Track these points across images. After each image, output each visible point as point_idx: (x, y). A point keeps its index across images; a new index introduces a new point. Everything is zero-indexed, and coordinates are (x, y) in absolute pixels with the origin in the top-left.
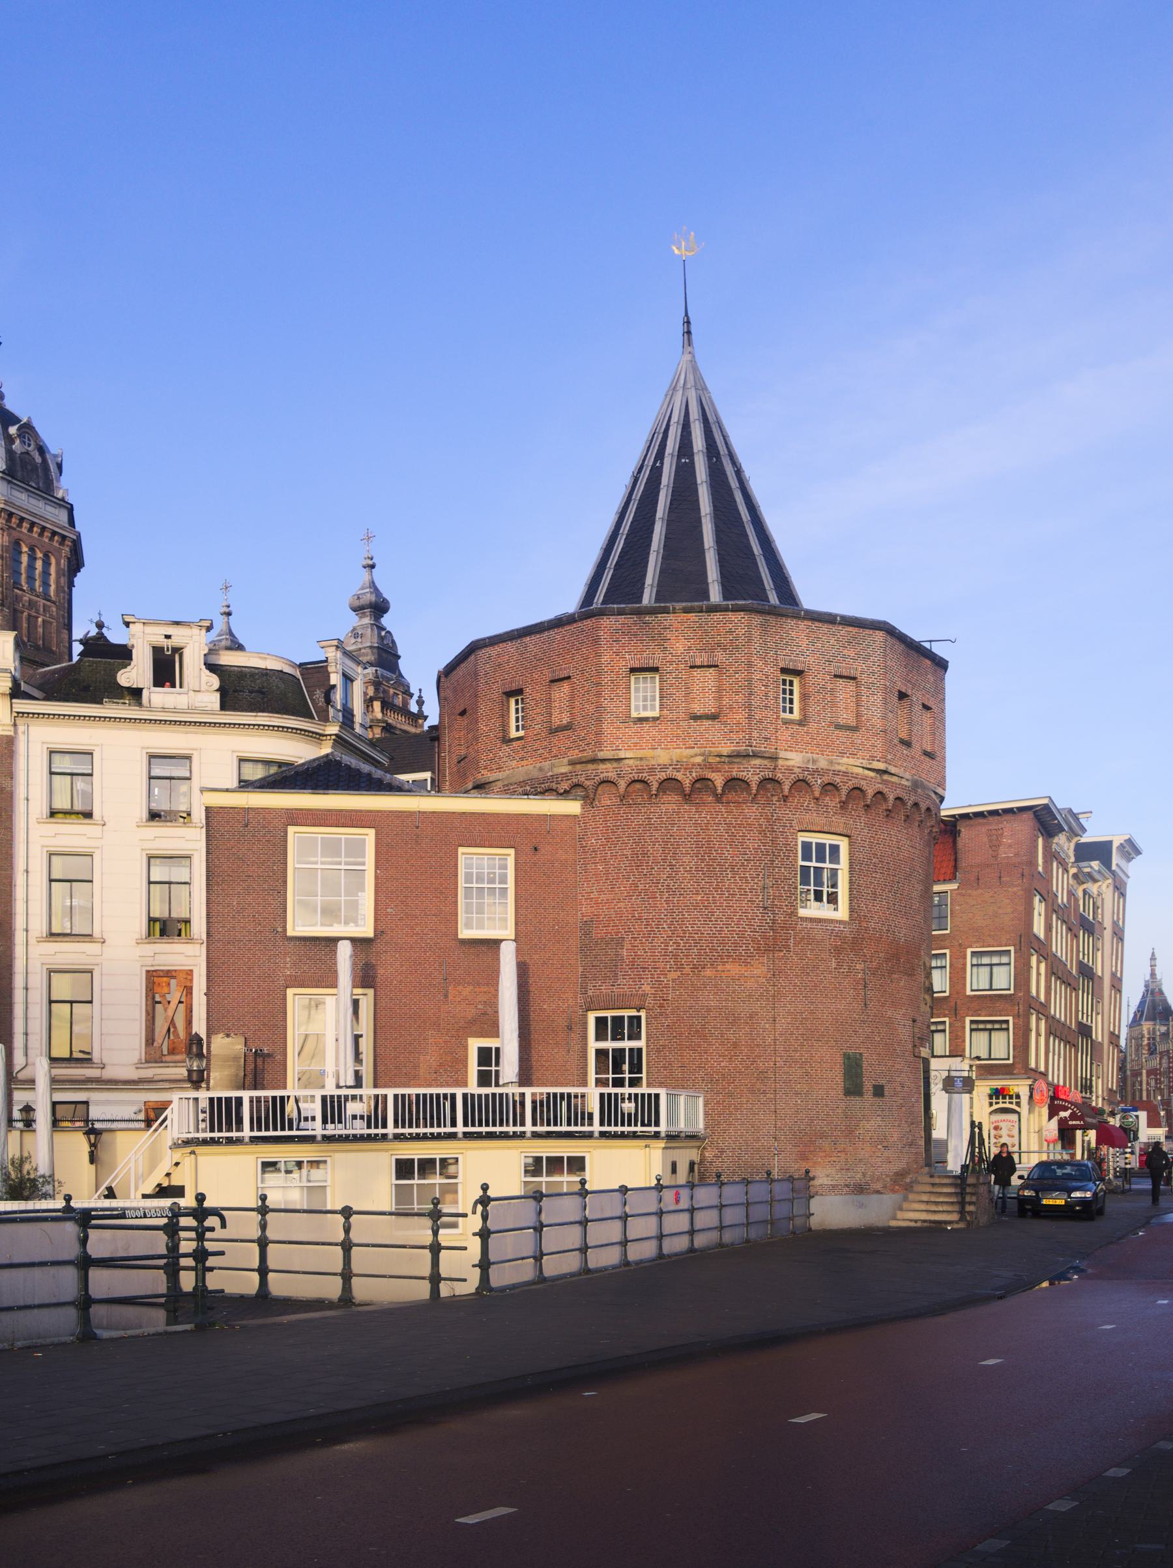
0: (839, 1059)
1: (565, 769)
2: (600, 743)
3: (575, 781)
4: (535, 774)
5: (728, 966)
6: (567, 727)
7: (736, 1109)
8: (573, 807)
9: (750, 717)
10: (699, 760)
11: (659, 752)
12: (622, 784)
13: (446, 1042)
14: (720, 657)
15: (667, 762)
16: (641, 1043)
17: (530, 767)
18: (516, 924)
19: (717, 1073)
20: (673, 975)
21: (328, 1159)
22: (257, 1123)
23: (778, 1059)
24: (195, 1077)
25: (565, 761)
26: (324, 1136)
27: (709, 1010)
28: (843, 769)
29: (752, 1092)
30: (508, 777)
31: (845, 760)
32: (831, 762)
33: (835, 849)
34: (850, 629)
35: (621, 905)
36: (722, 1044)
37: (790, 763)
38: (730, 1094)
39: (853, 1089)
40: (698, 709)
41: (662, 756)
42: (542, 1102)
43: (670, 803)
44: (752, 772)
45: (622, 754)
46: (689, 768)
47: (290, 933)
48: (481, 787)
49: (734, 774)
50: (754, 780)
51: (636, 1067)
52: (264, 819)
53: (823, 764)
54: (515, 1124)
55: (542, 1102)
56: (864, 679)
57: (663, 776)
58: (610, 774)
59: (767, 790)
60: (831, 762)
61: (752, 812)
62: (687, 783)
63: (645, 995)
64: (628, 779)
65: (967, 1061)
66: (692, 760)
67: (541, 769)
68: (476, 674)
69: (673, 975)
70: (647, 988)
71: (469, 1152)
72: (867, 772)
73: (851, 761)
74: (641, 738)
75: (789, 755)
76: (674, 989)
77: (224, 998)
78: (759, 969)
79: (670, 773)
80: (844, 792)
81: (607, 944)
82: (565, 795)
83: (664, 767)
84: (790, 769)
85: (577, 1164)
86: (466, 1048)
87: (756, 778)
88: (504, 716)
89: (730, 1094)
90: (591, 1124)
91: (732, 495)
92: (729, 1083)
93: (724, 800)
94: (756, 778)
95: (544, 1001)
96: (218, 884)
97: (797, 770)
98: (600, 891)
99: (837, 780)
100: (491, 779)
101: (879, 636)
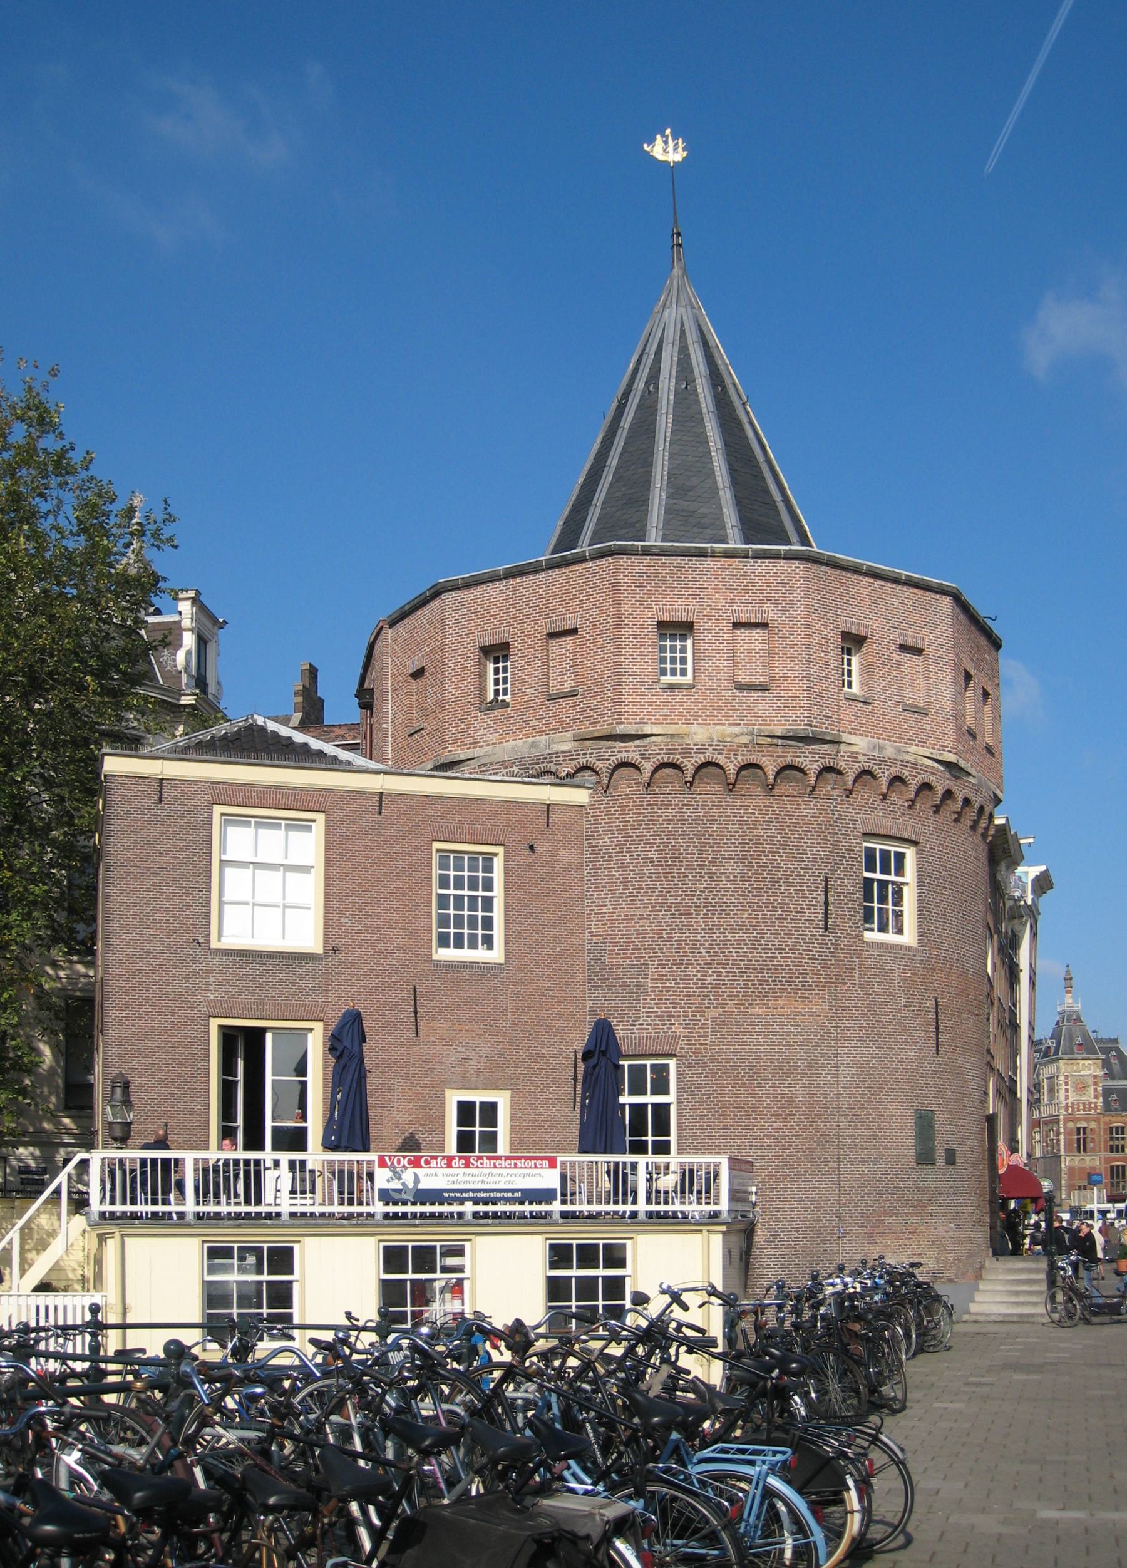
0: (910, 1119)
1: (566, 747)
2: (620, 714)
3: (582, 761)
4: (525, 752)
5: (781, 1002)
6: (571, 694)
7: (792, 1182)
8: (580, 796)
9: (809, 690)
10: (745, 739)
11: (694, 728)
12: (647, 767)
13: (417, 1094)
14: (771, 614)
15: (706, 742)
16: (670, 1098)
17: (519, 743)
18: (506, 944)
19: (769, 1136)
20: (712, 1013)
21: (467, 1245)
22: (203, 1192)
23: (842, 1119)
24: (118, 1132)
25: (570, 735)
26: (293, 1215)
27: (758, 1058)
28: (912, 759)
29: (812, 1161)
30: (486, 755)
31: (913, 749)
32: (899, 750)
33: (900, 857)
34: (916, 591)
35: (646, 923)
36: (775, 1100)
37: (854, 749)
38: (784, 1163)
39: (925, 1157)
40: (743, 677)
41: (699, 734)
42: (351, 1173)
43: (709, 792)
44: (810, 759)
45: (648, 730)
46: (734, 751)
47: (214, 944)
48: (446, 767)
49: (789, 759)
50: (813, 768)
51: (662, 1127)
52: (183, 793)
53: (889, 751)
54: (247, 1201)
55: (351, 1173)
56: (930, 650)
57: (701, 759)
58: (631, 755)
59: (827, 782)
60: (899, 750)
61: (808, 809)
62: (731, 769)
63: (675, 1038)
64: (655, 761)
65: (268, 1155)
66: (737, 740)
67: (533, 745)
68: (442, 621)
69: (712, 1013)
70: (678, 1029)
71: (307, 1239)
72: (936, 765)
73: (921, 750)
74: (673, 710)
75: (853, 739)
76: (713, 1030)
77: (127, 1028)
78: (820, 1006)
79: (710, 755)
80: (913, 788)
81: (625, 972)
82: (568, 780)
83: (702, 749)
84: (853, 756)
85: (615, 1257)
86: (442, 1102)
87: (815, 766)
88: (482, 676)
89: (784, 1163)
90: (634, 1202)
91: (743, 430)
92: (784, 1149)
93: (776, 791)
94: (815, 766)
95: (543, 1044)
96: (121, 878)
97: (861, 758)
98: (616, 905)
99: (906, 773)
100: (462, 757)
101: (949, 599)
